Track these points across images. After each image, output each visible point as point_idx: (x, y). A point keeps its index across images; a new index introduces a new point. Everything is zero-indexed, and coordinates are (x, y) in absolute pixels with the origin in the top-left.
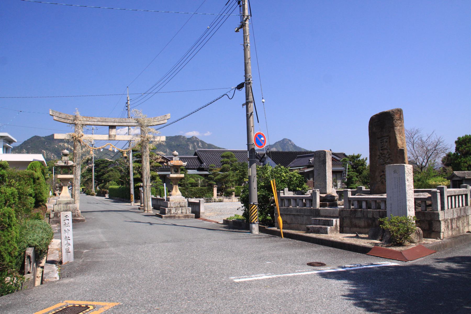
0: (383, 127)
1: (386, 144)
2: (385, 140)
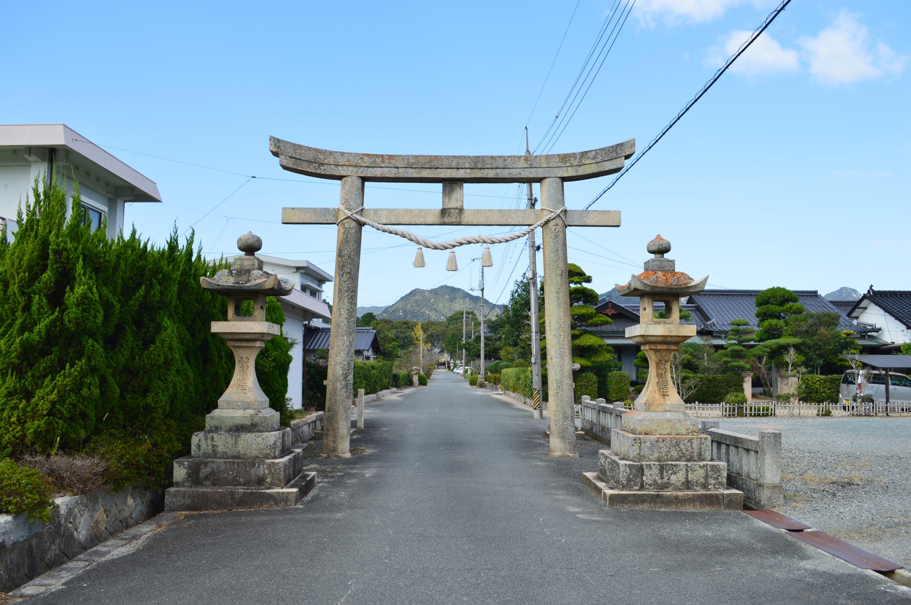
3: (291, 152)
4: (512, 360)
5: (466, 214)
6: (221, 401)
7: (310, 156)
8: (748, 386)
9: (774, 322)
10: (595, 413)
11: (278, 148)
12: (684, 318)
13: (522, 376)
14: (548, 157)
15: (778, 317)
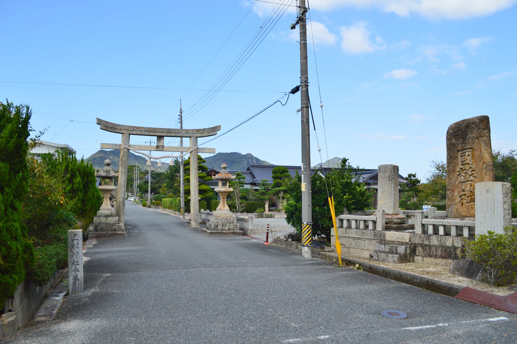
0: (468, 134)
1: (469, 158)
2: (467, 154)
3: (105, 124)
4: (166, 194)
5: (165, 148)
6: (101, 208)
7: (111, 126)
8: (267, 206)
9: (278, 180)
10: (205, 215)
11: (100, 122)
12: (230, 187)
13: (174, 202)
14: (193, 130)
15: (281, 178)
